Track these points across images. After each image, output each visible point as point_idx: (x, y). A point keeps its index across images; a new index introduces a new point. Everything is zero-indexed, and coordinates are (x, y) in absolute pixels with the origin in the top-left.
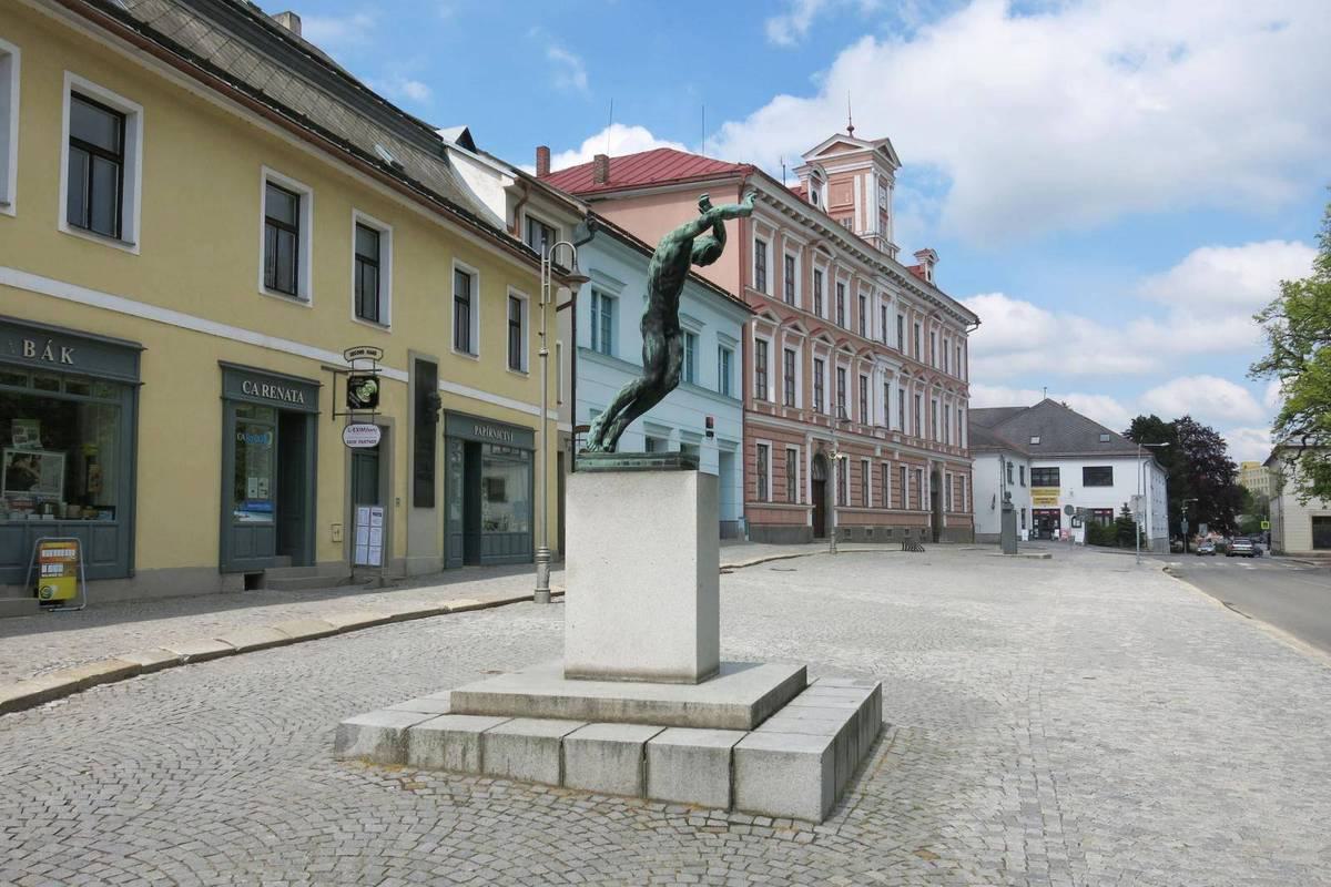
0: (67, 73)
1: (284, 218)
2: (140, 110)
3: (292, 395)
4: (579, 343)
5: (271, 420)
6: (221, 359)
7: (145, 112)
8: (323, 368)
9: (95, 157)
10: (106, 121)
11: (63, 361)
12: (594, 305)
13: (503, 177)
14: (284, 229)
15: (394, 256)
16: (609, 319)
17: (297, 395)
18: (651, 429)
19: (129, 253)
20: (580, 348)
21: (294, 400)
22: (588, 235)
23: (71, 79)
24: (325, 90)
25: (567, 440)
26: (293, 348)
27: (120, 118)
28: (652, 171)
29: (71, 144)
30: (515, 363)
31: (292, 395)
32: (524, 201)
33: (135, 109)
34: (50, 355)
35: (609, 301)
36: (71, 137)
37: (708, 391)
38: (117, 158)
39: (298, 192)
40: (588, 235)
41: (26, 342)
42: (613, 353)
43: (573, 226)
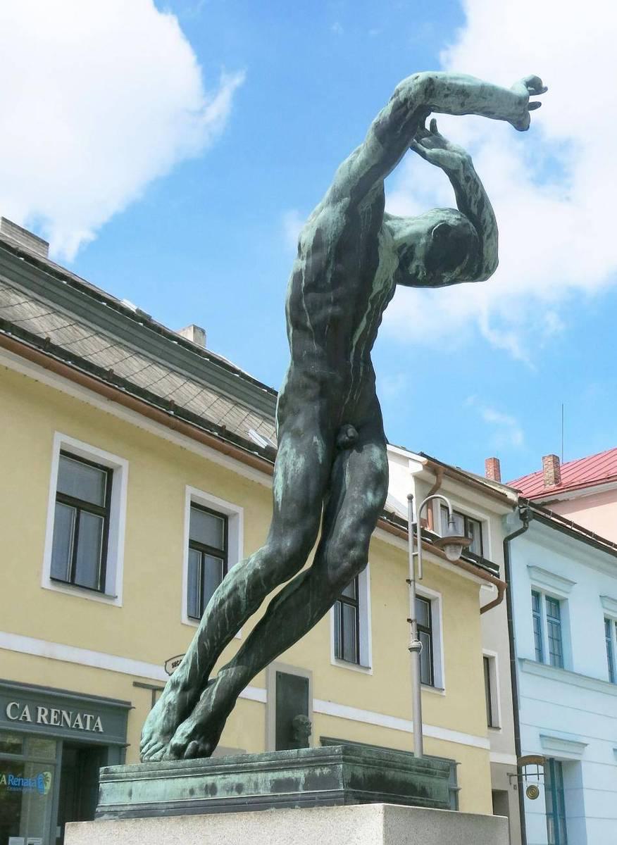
0: (188, 487)
1: (210, 539)
2: (240, 510)
3: (84, 720)
4: (519, 653)
5: (53, 753)
6: (322, 736)
7: (130, 466)
8: (136, 684)
9: (344, 604)
10: (94, 475)
11: (39, 721)
12: (537, 608)
13: (410, 461)
14: (86, 509)
15: (245, 541)
16: (559, 625)
17: (93, 721)
18: (549, 745)
19: (366, 674)
20: (522, 660)
21: (89, 728)
22: (520, 526)
23: (61, 440)
24: (193, 377)
25: (511, 775)
26: (91, 658)
27: (108, 473)
28: (609, 468)
29: (57, 500)
30: (428, 677)
31: (84, 720)
32: (436, 488)
33: (437, 596)
34: (100, 726)
35: (555, 603)
36: (58, 493)
37: (604, 682)
38: (104, 512)
39: (429, 597)
40: (520, 526)
41: (40, 709)
42: (566, 667)
43: (503, 517)
